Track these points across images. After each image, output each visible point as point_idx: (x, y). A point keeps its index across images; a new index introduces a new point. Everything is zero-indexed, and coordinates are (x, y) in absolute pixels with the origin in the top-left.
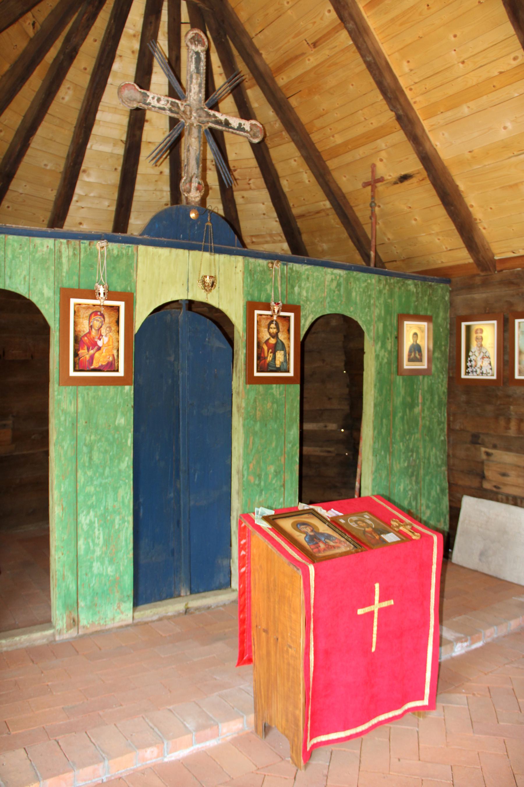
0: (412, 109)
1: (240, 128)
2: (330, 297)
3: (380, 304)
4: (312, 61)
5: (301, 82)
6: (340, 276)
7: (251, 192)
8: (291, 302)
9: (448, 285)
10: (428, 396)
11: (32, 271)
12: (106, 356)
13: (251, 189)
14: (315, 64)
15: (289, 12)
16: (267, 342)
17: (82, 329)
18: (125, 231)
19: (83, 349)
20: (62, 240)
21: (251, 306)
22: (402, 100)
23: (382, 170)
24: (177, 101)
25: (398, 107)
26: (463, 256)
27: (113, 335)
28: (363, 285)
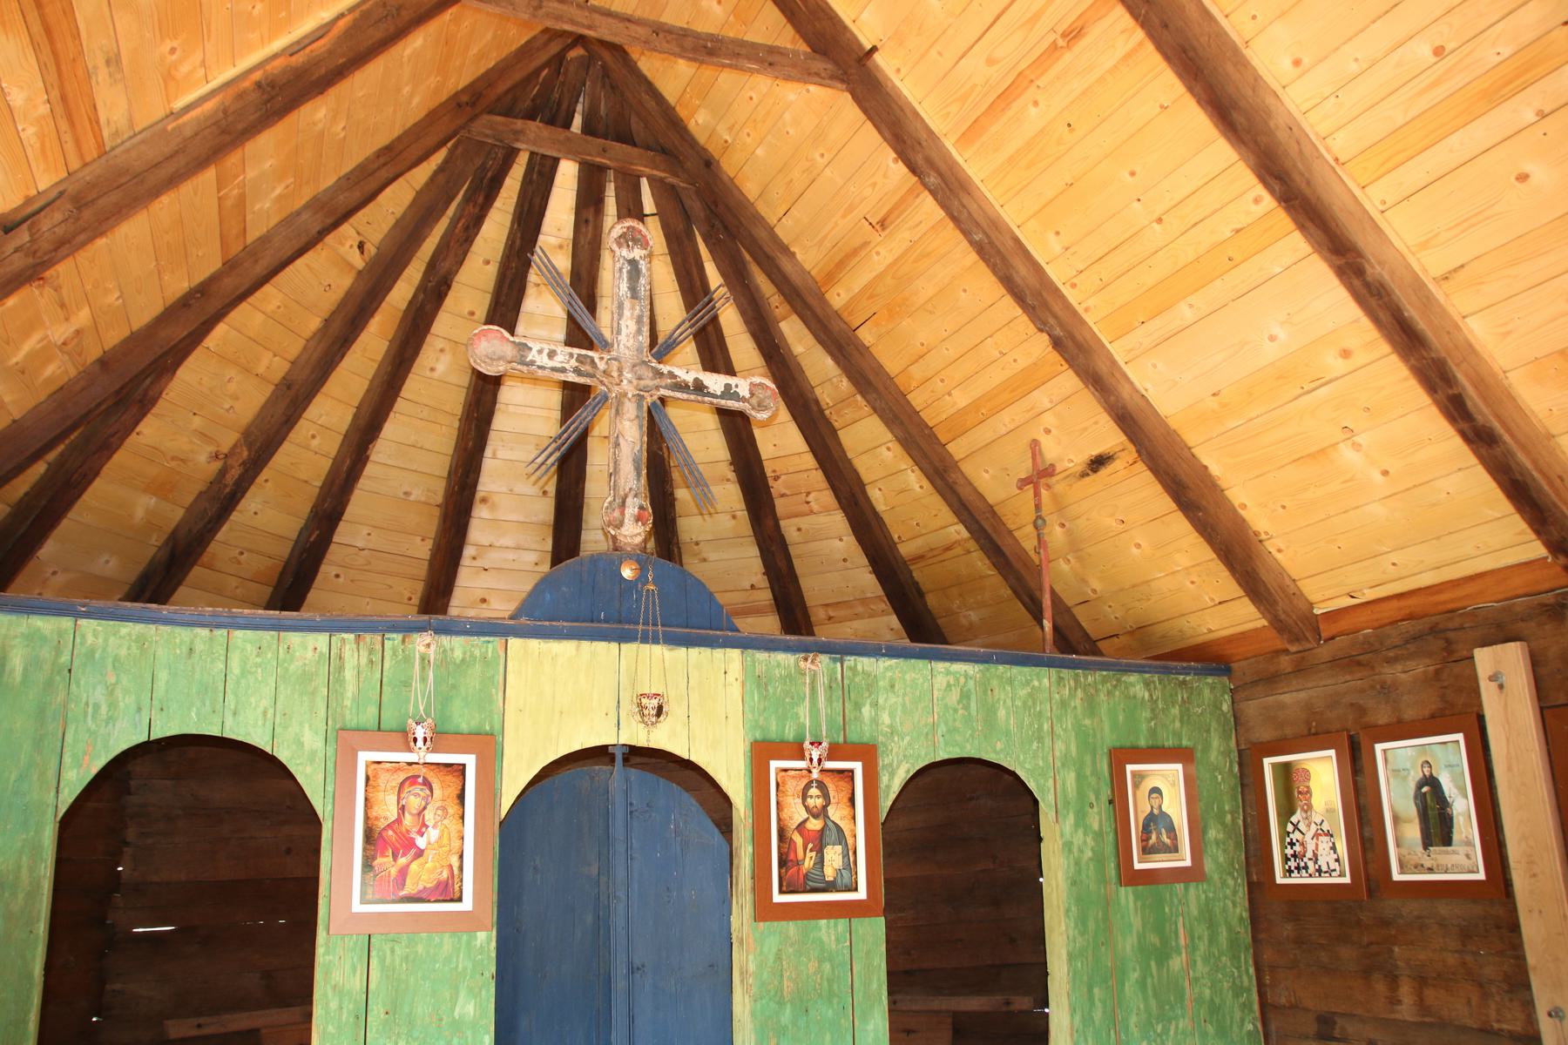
0: (1083, 323)
1: (699, 387)
2: (946, 724)
3: (1065, 730)
4: (883, 254)
5: (871, 297)
6: (966, 676)
7: (812, 518)
8: (853, 737)
9: (1225, 679)
10: (1202, 930)
11: (281, 698)
12: (435, 868)
13: (812, 512)
14: (889, 260)
15: (828, 172)
16: (801, 827)
17: (382, 814)
18: (444, 610)
19: (383, 855)
20: (345, 635)
21: (762, 752)
22: (1057, 307)
23: (1052, 450)
24: (590, 353)
25: (1052, 321)
26: (1242, 616)
27: (451, 824)
28: (1023, 692)
